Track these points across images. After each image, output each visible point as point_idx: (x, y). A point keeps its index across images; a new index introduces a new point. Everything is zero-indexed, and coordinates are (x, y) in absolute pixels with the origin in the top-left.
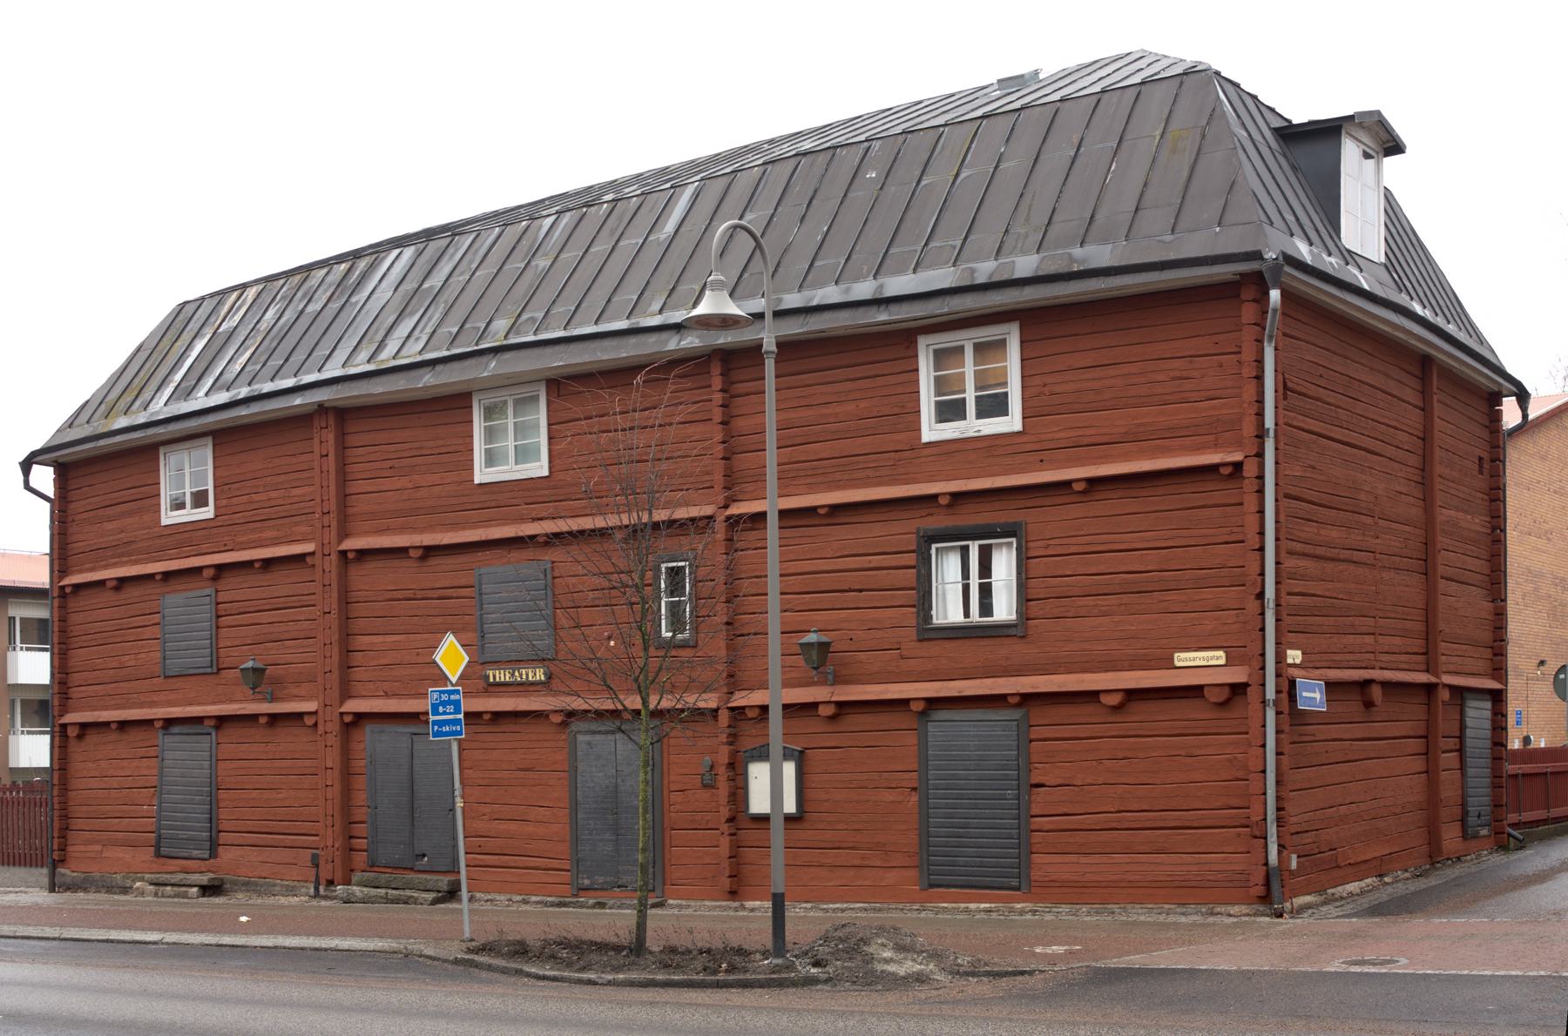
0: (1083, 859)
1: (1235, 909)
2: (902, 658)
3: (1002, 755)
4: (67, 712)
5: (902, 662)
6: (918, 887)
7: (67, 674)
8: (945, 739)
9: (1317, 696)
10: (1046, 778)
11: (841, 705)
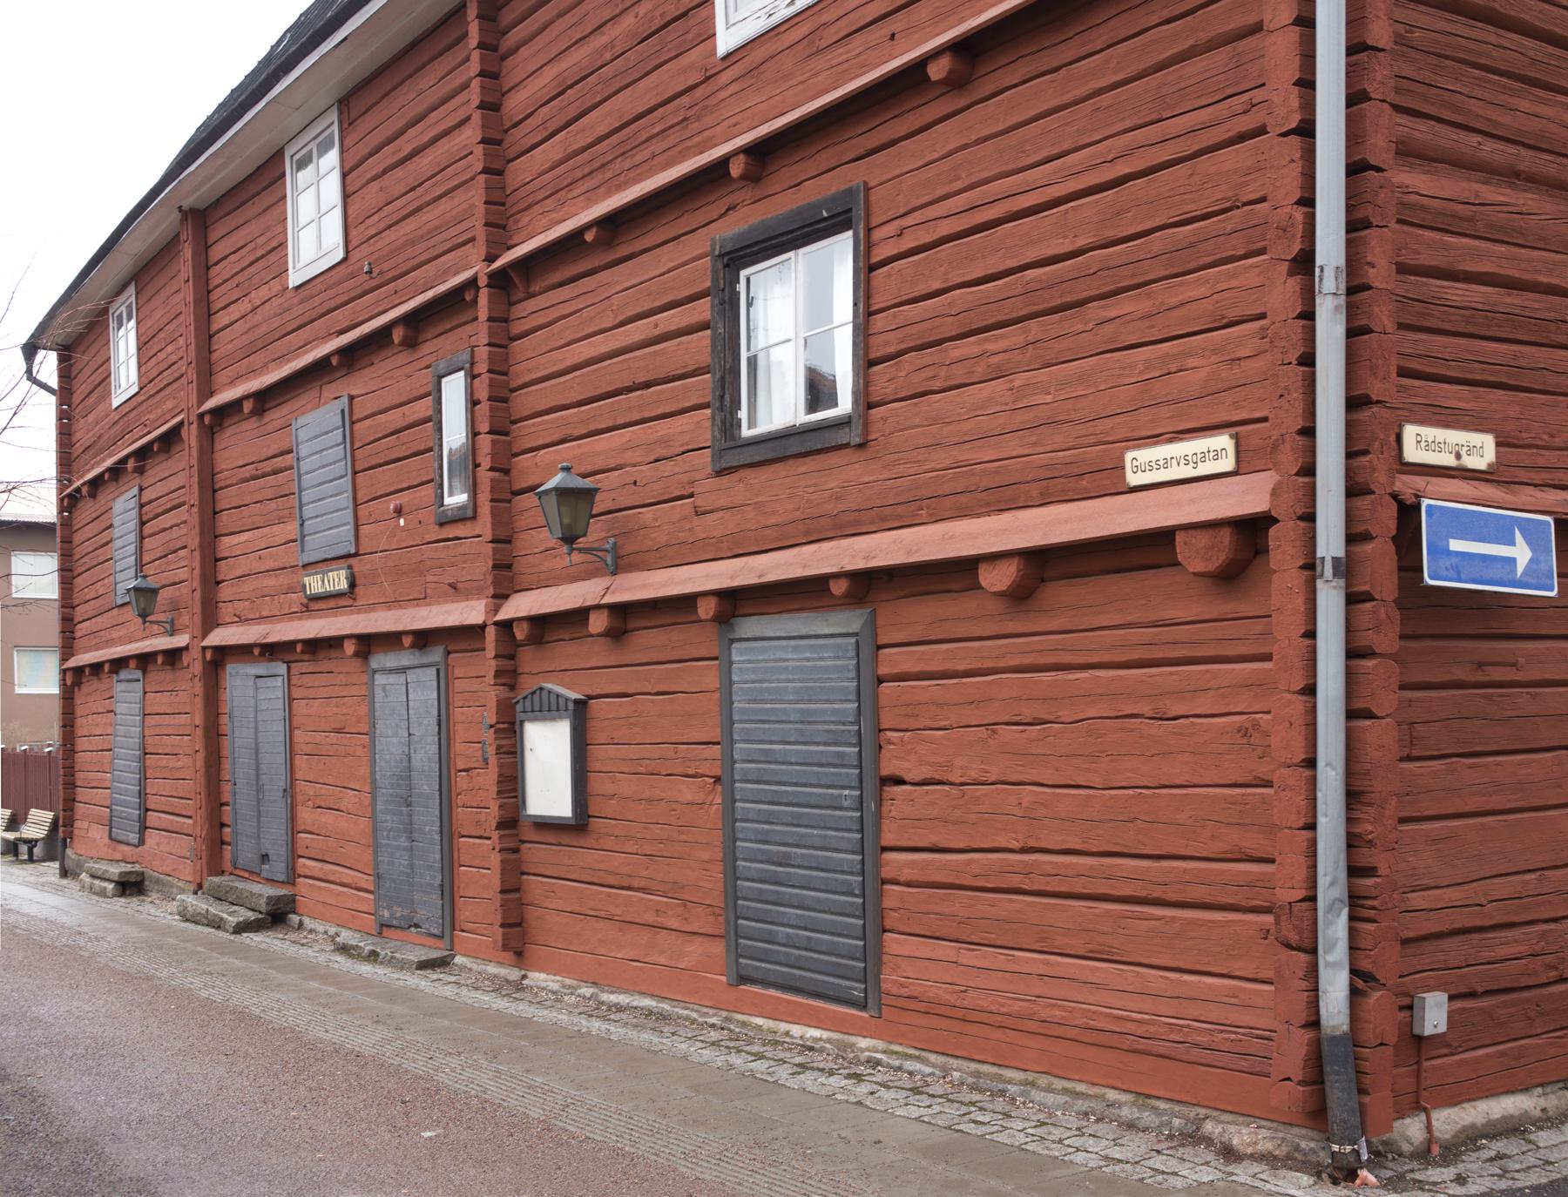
0: (968, 956)
1: (1242, 1136)
2: (698, 514)
3: (835, 711)
4: (73, 655)
5: (697, 521)
6: (724, 979)
7: (74, 608)
8: (753, 677)
9: (1521, 553)
10: (905, 764)
11: (622, 611)
